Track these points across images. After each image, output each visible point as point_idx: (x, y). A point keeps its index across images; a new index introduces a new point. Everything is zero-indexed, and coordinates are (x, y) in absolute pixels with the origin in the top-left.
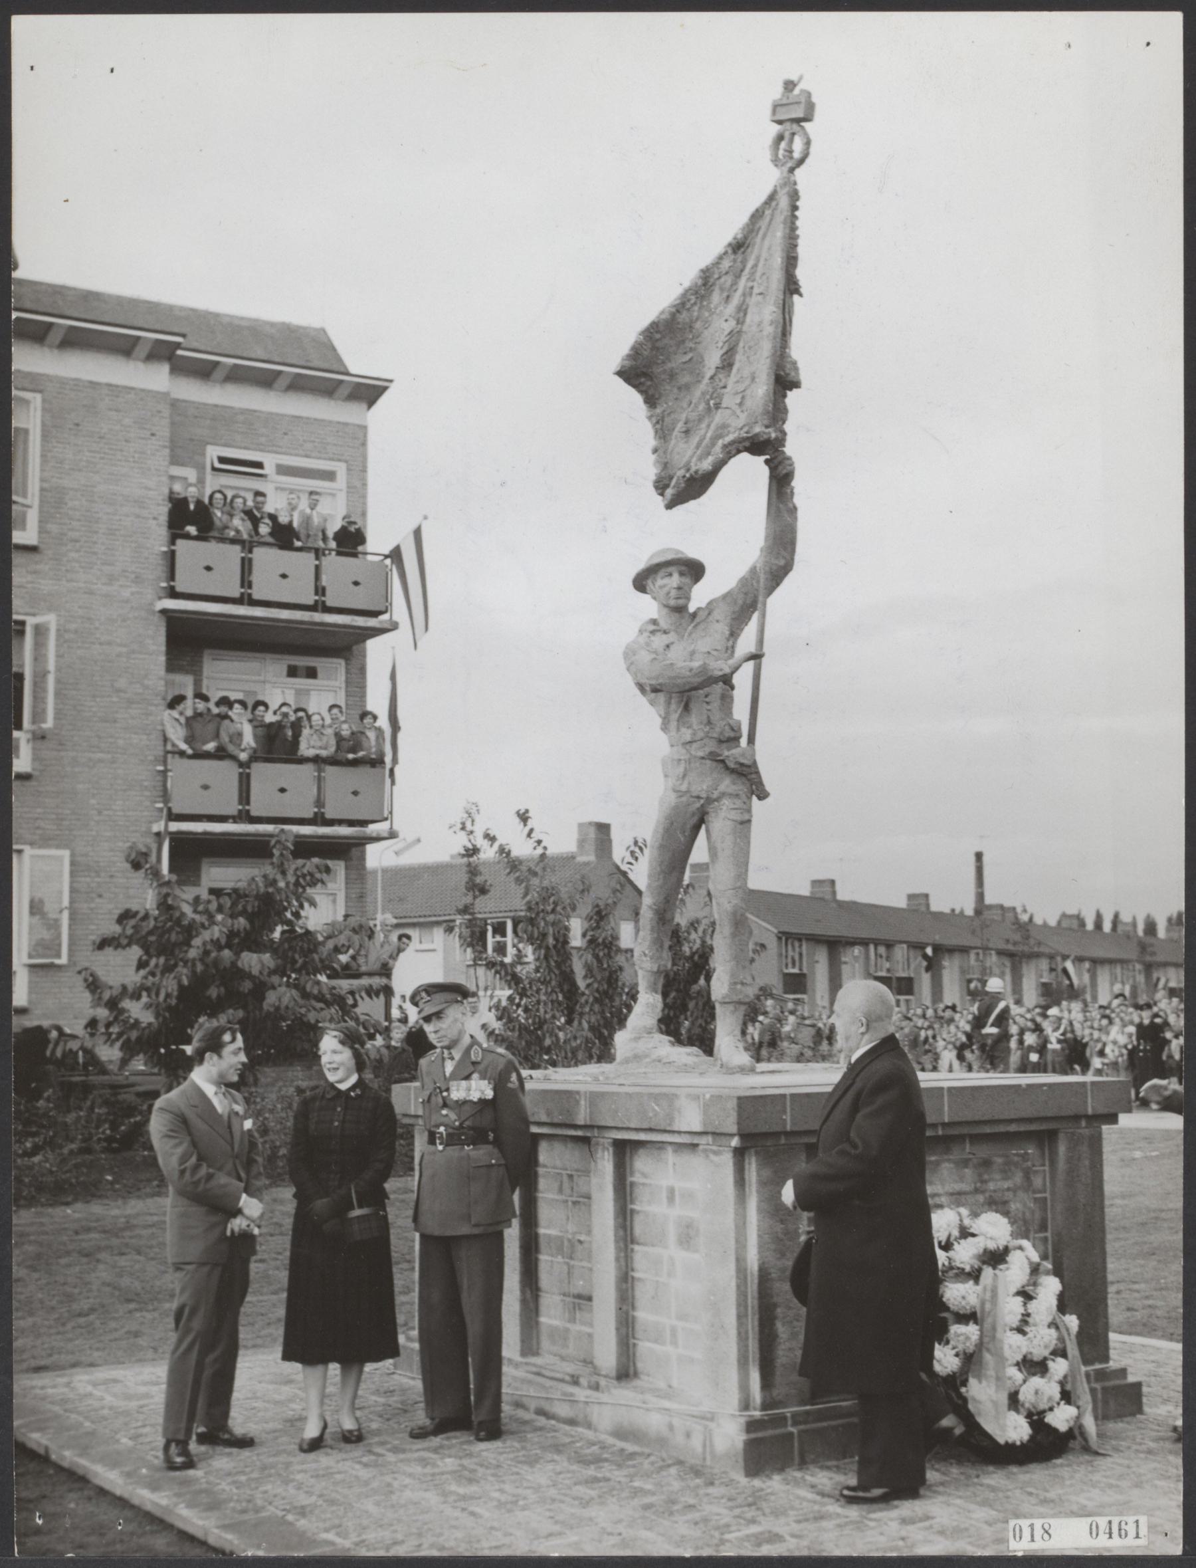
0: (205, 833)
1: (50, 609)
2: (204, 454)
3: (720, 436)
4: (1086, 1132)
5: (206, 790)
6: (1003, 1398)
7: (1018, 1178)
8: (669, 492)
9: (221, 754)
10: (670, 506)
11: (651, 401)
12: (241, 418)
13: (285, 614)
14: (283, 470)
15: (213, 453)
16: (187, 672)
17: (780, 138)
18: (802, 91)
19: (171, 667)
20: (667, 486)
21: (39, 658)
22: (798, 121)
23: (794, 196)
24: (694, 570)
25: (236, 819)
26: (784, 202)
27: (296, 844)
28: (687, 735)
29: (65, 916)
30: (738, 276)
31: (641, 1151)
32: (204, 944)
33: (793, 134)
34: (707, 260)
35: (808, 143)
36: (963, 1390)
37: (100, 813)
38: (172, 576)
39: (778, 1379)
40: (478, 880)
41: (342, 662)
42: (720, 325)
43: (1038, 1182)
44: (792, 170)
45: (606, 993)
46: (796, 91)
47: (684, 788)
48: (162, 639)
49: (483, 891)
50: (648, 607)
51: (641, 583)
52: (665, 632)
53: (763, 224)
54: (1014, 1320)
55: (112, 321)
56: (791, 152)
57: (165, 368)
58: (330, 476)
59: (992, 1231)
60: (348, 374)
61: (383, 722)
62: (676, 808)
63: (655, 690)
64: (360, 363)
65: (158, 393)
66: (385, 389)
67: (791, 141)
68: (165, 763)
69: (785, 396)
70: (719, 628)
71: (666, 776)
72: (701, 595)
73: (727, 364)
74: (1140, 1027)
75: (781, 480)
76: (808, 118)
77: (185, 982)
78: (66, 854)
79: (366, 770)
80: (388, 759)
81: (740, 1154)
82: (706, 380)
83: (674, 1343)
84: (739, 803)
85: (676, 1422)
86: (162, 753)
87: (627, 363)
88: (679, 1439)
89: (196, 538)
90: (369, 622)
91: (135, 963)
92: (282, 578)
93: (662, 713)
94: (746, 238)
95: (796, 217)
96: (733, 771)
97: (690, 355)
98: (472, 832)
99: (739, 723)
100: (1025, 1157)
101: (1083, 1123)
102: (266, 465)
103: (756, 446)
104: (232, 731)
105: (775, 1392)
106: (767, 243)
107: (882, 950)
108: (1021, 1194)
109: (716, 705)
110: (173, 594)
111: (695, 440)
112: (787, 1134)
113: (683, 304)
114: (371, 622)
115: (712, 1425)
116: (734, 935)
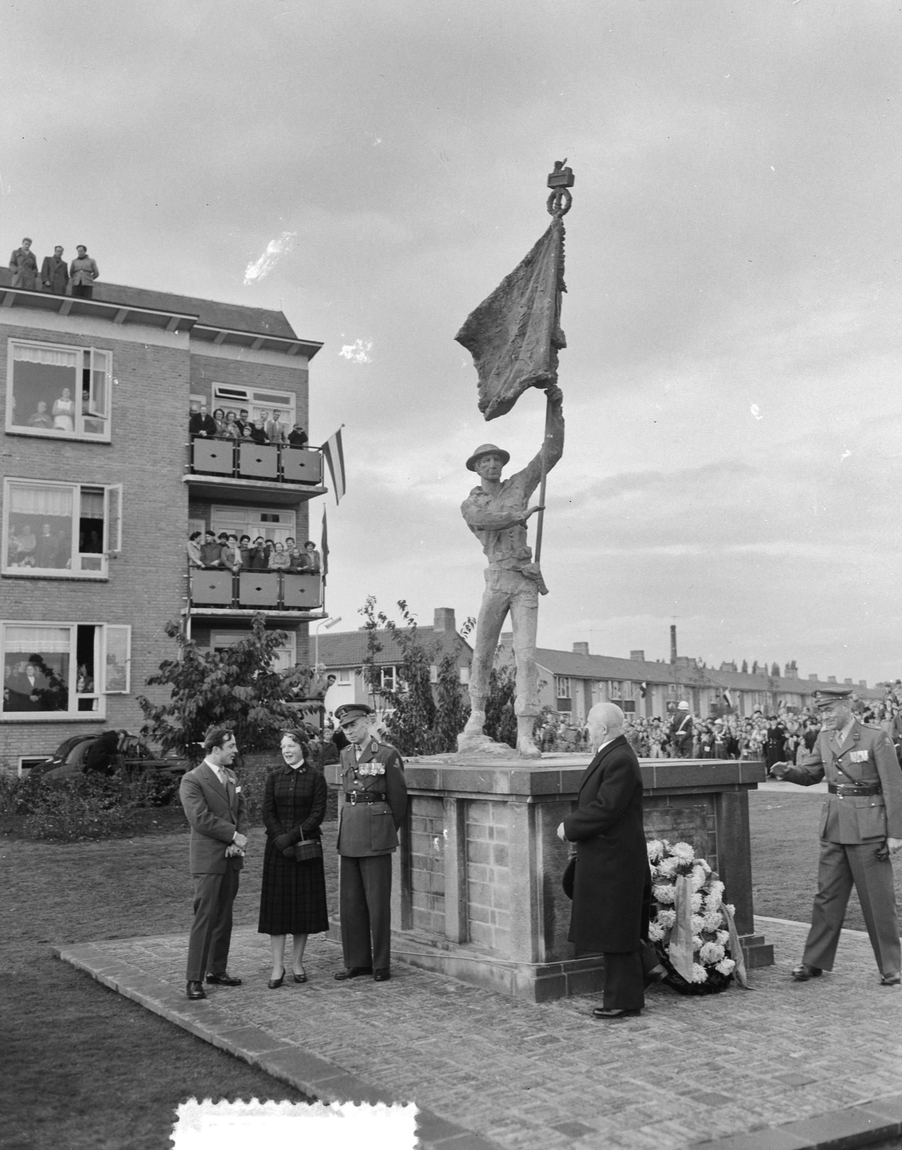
1: (119, 481)
2: (211, 388)
3: (518, 377)
5: (214, 589)
6: (691, 955)
7: (698, 822)
9: (222, 567)
11: (476, 356)
12: (232, 365)
13: (260, 483)
14: (257, 397)
15: (216, 386)
16: (202, 518)
17: (552, 197)
18: (566, 168)
19: (192, 516)
22: (564, 186)
23: (562, 232)
24: (503, 457)
25: (230, 606)
26: (556, 235)
27: (267, 621)
28: (499, 556)
30: (529, 281)
32: (212, 681)
33: (561, 195)
34: (509, 271)
35: (570, 200)
36: (666, 950)
37: (149, 603)
38: (192, 461)
40: (376, 643)
41: (294, 512)
42: (519, 311)
43: (710, 824)
44: (560, 216)
45: (452, 710)
46: (563, 169)
47: (497, 588)
48: (186, 499)
49: (379, 649)
50: (475, 480)
51: (472, 465)
52: (486, 494)
53: (543, 249)
57: (187, 336)
58: (286, 400)
59: (683, 854)
61: (319, 548)
64: (303, 333)
66: (319, 348)
67: (560, 198)
68: (188, 573)
69: (557, 352)
71: (487, 580)
72: (507, 472)
73: (522, 334)
74: (770, 730)
77: (201, 704)
78: (129, 627)
80: (322, 570)
81: (532, 807)
82: (509, 343)
83: (494, 922)
84: (530, 597)
85: (495, 969)
88: (497, 979)
89: (206, 438)
90: (312, 487)
91: (170, 693)
92: (258, 462)
94: (533, 257)
95: (563, 245)
96: (526, 578)
99: (530, 549)
100: (702, 809)
101: (737, 789)
102: (248, 394)
103: (539, 383)
104: (228, 553)
105: (554, 951)
106: (545, 261)
107: (616, 684)
108: (700, 831)
109: (516, 538)
110: (193, 471)
112: (560, 795)
113: (496, 297)
114: (311, 488)
115: (516, 971)
116: (528, 676)
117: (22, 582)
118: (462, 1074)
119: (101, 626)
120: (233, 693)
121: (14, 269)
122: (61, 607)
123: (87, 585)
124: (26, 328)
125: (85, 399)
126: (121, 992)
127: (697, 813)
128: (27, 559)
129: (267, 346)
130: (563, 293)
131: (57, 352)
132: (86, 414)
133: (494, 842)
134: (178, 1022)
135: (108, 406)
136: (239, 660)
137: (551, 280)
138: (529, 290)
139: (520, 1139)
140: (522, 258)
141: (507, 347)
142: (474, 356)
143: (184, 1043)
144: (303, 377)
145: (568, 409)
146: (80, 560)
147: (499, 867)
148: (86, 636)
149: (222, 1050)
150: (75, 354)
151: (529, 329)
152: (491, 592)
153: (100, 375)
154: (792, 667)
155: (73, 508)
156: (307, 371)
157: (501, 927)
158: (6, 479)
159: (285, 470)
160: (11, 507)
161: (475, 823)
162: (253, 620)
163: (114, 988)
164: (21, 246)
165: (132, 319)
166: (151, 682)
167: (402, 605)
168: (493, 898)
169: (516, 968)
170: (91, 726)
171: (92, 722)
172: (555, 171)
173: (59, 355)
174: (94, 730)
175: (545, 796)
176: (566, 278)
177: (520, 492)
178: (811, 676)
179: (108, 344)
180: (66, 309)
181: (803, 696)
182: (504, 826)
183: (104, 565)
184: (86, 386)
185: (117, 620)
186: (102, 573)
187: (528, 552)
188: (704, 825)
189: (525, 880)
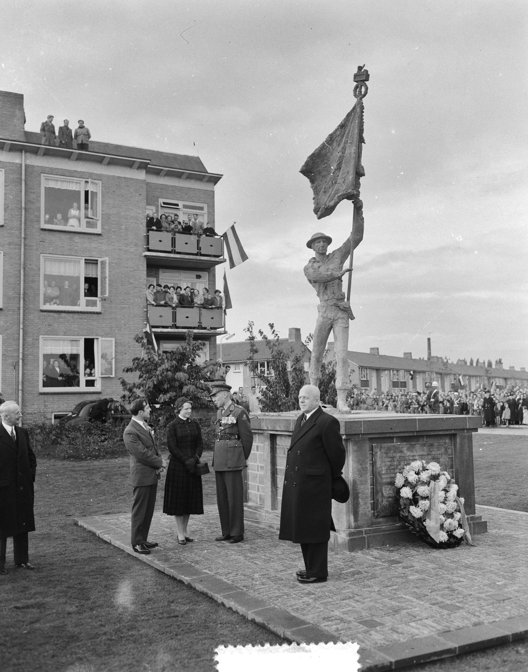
0: (161, 332)
5: (162, 317)
6: (438, 525)
7: (443, 450)
9: (166, 305)
10: (319, 218)
11: (312, 181)
13: (187, 257)
14: (185, 207)
15: (161, 201)
16: (154, 277)
17: (357, 87)
19: (148, 276)
21: (103, 272)
22: (363, 81)
23: (362, 108)
24: (328, 240)
25: (171, 327)
26: (358, 110)
27: (194, 336)
29: (114, 360)
33: (362, 86)
34: (331, 132)
35: (367, 89)
36: (424, 523)
39: (360, 518)
40: (255, 348)
42: (337, 155)
43: (450, 451)
44: (361, 99)
47: (325, 316)
48: (145, 266)
49: (256, 351)
50: (312, 253)
51: (310, 245)
52: (318, 262)
53: (351, 118)
54: (442, 499)
58: (202, 209)
59: (434, 469)
60: (207, 173)
64: (211, 169)
66: (221, 178)
67: (361, 88)
70: (338, 261)
71: (319, 312)
72: (330, 249)
73: (339, 168)
74: (485, 399)
76: (367, 80)
77: (156, 383)
78: (114, 339)
80: (224, 307)
84: (344, 321)
89: (156, 230)
92: (186, 244)
94: (345, 123)
95: (363, 116)
96: (342, 310)
98: (251, 332)
100: (445, 443)
103: (349, 197)
105: (359, 523)
106: (353, 125)
107: (395, 372)
108: (444, 456)
109: (336, 287)
110: (149, 250)
113: (323, 147)
114: (217, 259)
117: (52, 314)
119: (97, 339)
121: (43, 133)
123: (90, 315)
125: (86, 208)
126: (112, 544)
127: (442, 445)
128: (54, 301)
129: (190, 177)
131: (70, 182)
139: (340, 628)
140: (339, 123)
142: (310, 182)
144: (211, 195)
145: (366, 213)
146: (85, 301)
148: (89, 344)
149: (170, 576)
150: (80, 183)
153: (94, 194)
154: (499, 362)
155: (80, 271)
158: (42, 255)
163: (109, 541)
164: (47, 120)
165: (112, 163)
167: (272, 326)
176: (364, 135)
179: (99, 177)
180: (74, 157)
181: (506, 379)
183: (99, 304)
184: (86, 201)
185: (107, 335)
186: (98, 309)
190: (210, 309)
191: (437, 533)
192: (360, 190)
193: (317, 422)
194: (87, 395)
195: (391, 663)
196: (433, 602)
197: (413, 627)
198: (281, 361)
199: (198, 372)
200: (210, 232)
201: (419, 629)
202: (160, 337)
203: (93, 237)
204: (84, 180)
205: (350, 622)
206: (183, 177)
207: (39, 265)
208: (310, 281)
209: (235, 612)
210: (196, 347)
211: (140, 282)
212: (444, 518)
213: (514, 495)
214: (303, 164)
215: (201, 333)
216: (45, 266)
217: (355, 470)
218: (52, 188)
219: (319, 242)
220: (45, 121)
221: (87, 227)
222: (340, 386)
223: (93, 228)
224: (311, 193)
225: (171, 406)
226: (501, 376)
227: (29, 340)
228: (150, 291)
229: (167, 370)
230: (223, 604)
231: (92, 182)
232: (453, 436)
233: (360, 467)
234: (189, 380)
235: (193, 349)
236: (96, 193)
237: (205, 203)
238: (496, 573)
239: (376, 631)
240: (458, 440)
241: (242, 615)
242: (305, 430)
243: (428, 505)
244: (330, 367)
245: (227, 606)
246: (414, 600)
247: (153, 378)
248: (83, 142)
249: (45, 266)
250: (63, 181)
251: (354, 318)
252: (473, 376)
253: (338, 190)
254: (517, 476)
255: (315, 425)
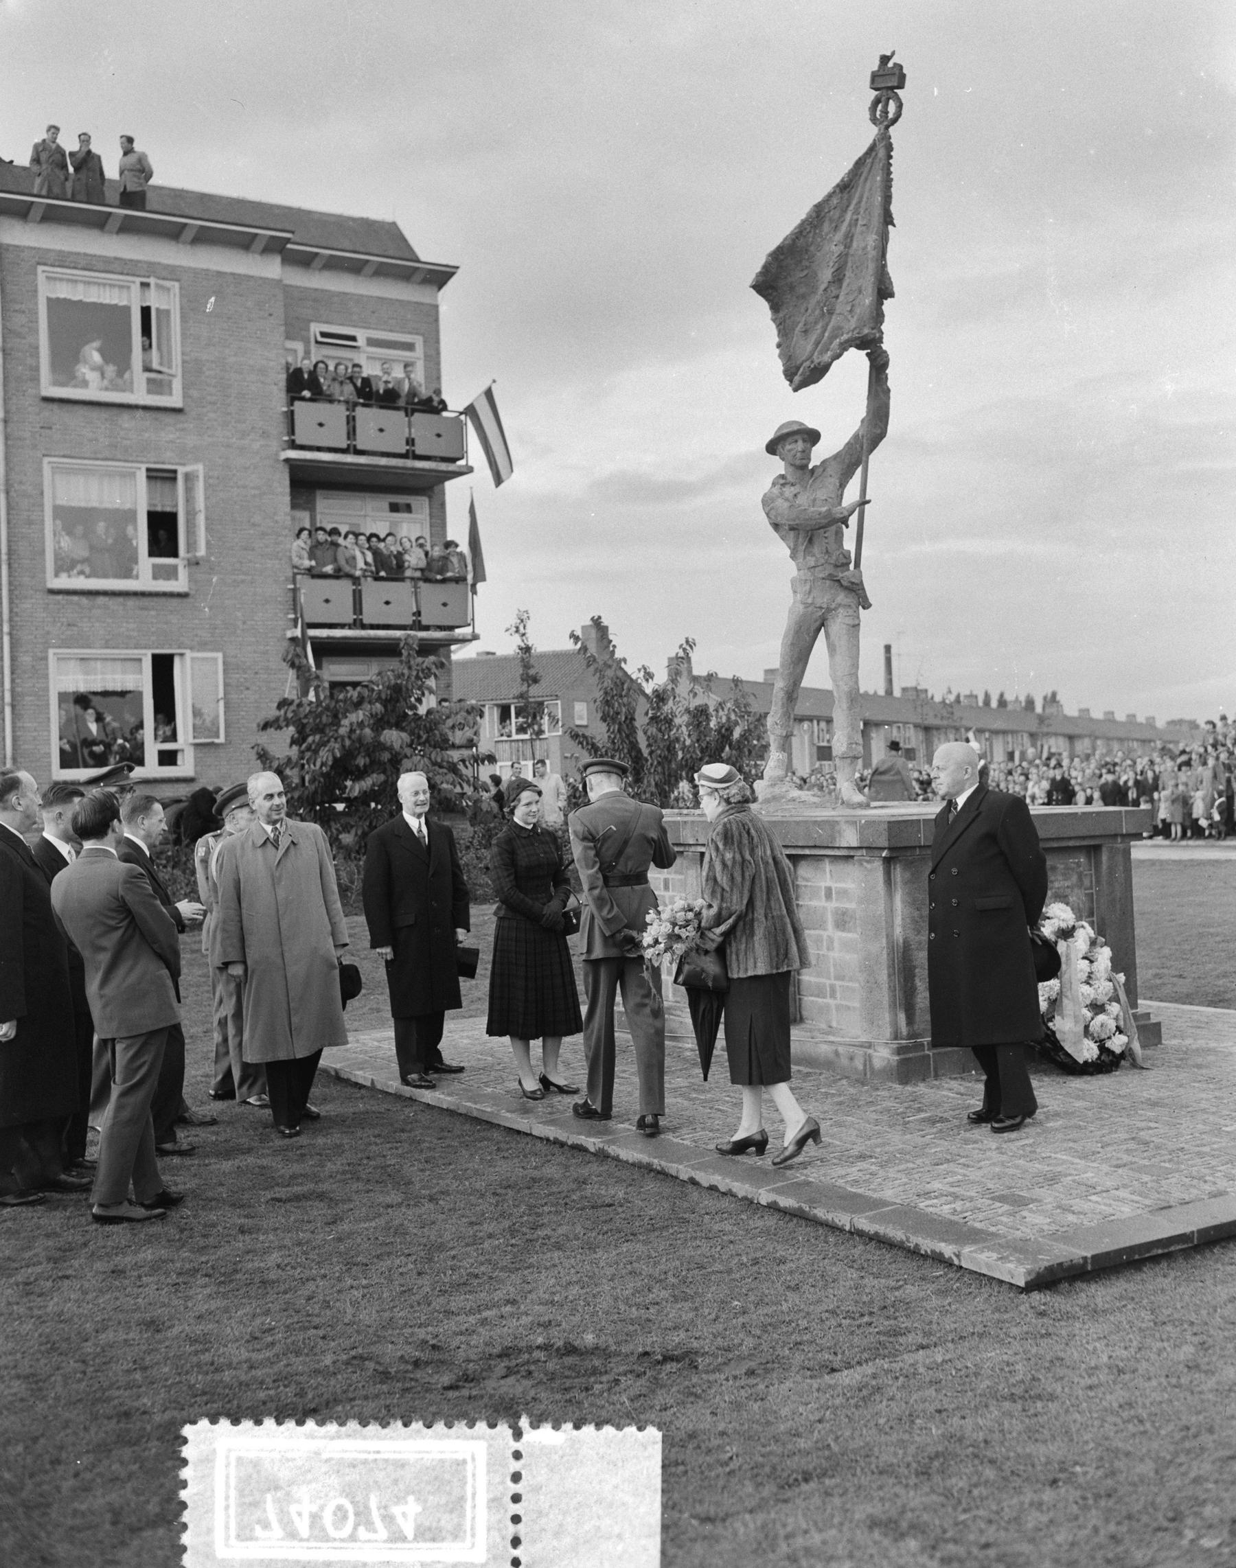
0: (328, 638)
1: (197, 460)
2: (309, 330)
3: (836, 337)
4: (1121, 846)
5: (329, 603)
6: (1081, 1029)
7: (1074, 878)
8: (797, 379)
9: (338, 575)
10: (795, 390)
11: (775, 308)
12: (336, 299)
13: (383, 461)
14: (372, 342)
15: (316, 328)
16: (305, 509)
17: (877, 102)
18: (895, 64)
19: (294, 506)
20: (796, 374)
21: (189, 499)
22: (892, 88)
23: (890, 148)
24: (813, 437)
25: (350, 627)
26: (882, 153)
27: (420, 645)
28: (811, 561)
29: (222, 704)
30: (845, 211)
31: (803, 863)
32: (351, 724)
33: (888, 99)
34: (819, 197)
35: (900, 106)
36: (1050, 1024)
37: (244, 623)
38: (292, 431)
39: (917, 1019)
40: (532, 672)
41: (427, 500)
42: (832, 248)
43: (1087, 882)
44: (887, 128)
45: (666, 758)
46: (890, 64)
47: (810, 601)
48: (287, 482)
49: (535, 680)
50: (777, 466)
51: (772, 448)
52: (792, 485)
53: (866, 170)
54: (1084, 977)
55: (221, 219)
56: (887, 113)
57: (278, 259)
58: (410, 347)
59: (1064, 916)
60: (418, 261)
61: (464, 547)
62: (804, 615)
63: (792, 529)
64: (429, 252)
65: (273, 280)
66: (453, 274)
67: (887, 104)
68: (294, 582)
69: (882, 304)
70: (833, 481)
71: (795, 592)
72: (819, 454)
73: (838, 279)
74: (1053, 781)
75: (879, 366)
76: (901, 86)
77: (338, 755)
78: (220, 655)
79: (453, 585)
80: (470, 577)
81: (888, 861)
82: (820, 291)
83: (833, 995)
84: (851, 612)
85: (841, 1049)
86: (291, 574)
87: (761, 279)
88: (844, 1061)
89: (311, 400)
90: (451, 464)
91: (289, 741)
92: (381, 431)
93: (792, 545)
94: (851, 181)
95: (890, 165)
96: (846, 588)
97: (805, 272)
98: (524, 635)
99: (849, 552)
100: (1078, 864)
101: (1119, 840)
102: (359, 338)
103: (861, 344)
104: (347, 555)
105: (916, 1027)
106: (868, 184)
107: (823, 725)
108: (1076, 890)
109: (832, 539)
110: (293, 445)
111: (813, 337)
112: (920, 847)
113: (801, 232)
114: (451, 467)
115: (870, 1051)
116: (850, 709)
117: (75, 598)
118: (855, 1152)
119: (182, 655)
120: (382, 738)
121: (36, 168)
122: (128, 630)
123: (163, 600)
124: (60, 251)
125: (147, 348)
126: (379, 1087)
127: (1073, 869)
128: (79, 567)
129: (382, 272)
130: (890, 227)
131: (104, 285)
132: (148, 369)
133: (833, 904)
134: (475, 1114)
135: (177, 359)
136: (383, 696)
137: (877, 212)
138: (846, 224)
139: (959, 1209)
140: (837, 180)
141: (818, 297)
142: (772, 308)
143: (496, 1135)
144: (432, 314)
145: (893, 374)
146: (150, 566)
147: (840, 933)
148: (163, 668)
149: (548, 1140)
150: (129, 288)
151: (848, 274)
152: (801, 607)
153: (165, 314)
154: (1052, 700)
155: (138, 498)
156: (436, 307)
157: (844, 1003)
158: (46, 460)
159: (416, 441)
160: (54, 498)
161: (804, 883)
162: (402, 645)
163: (368, 1084)
164: (45, 136)
165: (204, 238)
166: (265, 726)
168: (832, 970)
169: (869, 1047)
170: (176, 786)
171: (178, 780)
172: (880, 67)
173: (116, 290)
174: (184, 791)
175: (897, 849)
176: (893, 208)
177: (835, 481)
178: (1081, 711)
179: (172, 273)
180: (113, 224)
181: (1071, 738)
182: (849, 885)
183: (183, 573)
184: (146, 330)
185: (203, 646)
186: (179, 584)
187: (846, 555)
188: (1080, 884)
189: (879, 948)
190: (437, 581)
191: (1077, 1043)
192: (883, 327)
193: (982, 808)
194: (164, 786)
195: (1085, 1258)
196: (1115, 1163)
197: (1097, 1202)
198: (625, 700)
199: (431, 730)
200: (433, 406)
201: (1110, 1205)
202: (325, 650)
203: (160, 415)
204: (138, 280)
205: (971, 1199)
206: (183, 237)
207: (41, 484)
208: (776, 526)
209: (724, 1194)
210: (423, 670)
211: (277, 522)
212: (1089, 1015)
213: (1181, 976)
214: (758, 269)
215: (356, 638)
216: (54, 487)
217: (908, 920)
218: (65, 299)
219: (793, 441)
220: (38, 140)
221: (149, 392)
222: (844, 749)
223: (161, 394)
224: (771, 334)
225: (369, 806)
226: (1059, 731)
227: (26, 659)
228: (300, 542)
229: (361, 725)
230: (693, 1182)
231: (158, 286)
232: (1093, 851)
233: (916, 913)
234: (410, 746)
235: (417, 677)
236: (168, 312)
237: (417, 334)
238: (1213, 1113)
239: (1031, 1211)
240: (1104, 858)
241: (745, 1198)
242: (962, 826)
243: (1057, 988)
244: (721, 713)
245: (706, 1184)
246: (1077, 1161)
247: (332, 744)
248: (128, 189)
249: (54, 487)
250: (89, 283)
251: (870, 605)
252: (996, 732)
253: (838, 331)
254: (1178, 939)
255: (979, 814)
